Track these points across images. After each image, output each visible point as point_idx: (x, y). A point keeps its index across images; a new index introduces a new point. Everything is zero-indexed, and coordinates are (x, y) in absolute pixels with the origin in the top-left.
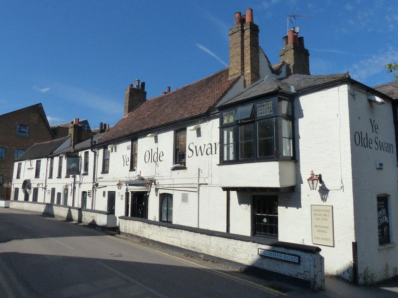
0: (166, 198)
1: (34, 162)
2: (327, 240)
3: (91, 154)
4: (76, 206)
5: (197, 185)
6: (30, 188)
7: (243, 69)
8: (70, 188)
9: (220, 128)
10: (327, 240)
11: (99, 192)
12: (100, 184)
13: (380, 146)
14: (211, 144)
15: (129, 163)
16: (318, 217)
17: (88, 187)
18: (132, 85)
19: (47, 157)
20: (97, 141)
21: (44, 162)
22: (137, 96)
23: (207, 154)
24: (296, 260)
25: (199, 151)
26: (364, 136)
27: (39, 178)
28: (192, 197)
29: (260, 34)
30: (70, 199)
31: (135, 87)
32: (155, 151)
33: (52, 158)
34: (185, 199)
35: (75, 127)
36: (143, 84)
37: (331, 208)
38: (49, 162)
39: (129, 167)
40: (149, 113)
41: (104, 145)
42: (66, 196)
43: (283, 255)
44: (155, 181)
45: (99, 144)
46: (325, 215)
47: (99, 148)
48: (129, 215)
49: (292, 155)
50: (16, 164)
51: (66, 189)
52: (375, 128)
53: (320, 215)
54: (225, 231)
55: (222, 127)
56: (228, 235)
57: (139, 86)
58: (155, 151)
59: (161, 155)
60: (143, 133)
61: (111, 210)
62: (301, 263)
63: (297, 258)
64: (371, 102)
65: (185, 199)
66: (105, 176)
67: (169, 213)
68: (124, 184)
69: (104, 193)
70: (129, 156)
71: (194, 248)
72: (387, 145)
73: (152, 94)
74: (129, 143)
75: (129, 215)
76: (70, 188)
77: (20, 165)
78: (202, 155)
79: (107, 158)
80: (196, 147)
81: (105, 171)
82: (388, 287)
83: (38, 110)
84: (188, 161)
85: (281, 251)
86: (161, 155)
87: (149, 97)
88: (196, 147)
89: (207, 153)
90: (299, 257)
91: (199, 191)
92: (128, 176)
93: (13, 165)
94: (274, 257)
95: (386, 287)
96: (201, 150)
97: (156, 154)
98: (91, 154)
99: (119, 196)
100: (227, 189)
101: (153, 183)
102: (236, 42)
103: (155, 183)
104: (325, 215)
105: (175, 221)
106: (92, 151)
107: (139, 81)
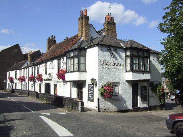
1: (15, 71)
3: (68, 60)
6: (13, 83)
7: (82, 34)
18: (49, 38)
19: (19, 69)
21: (18, 71)
22: (52, 42)
31: (51, 38)
33: (21, 70)
34: (60, 86)
35: (30, 55)
36: (55, 37)
38: (20, 71)
41: (46, 62)
45: (36, 64)
47: (36, 66)
50: (8, 73)
57: (52, 38)
72: (119, 64)
73: (58, 41)
77: (9, 73)
82: (45, 113)
83: (17, 47)
87: (57, 42)
93: (7, 73)
95: (43, 113)
107: (53, 36)
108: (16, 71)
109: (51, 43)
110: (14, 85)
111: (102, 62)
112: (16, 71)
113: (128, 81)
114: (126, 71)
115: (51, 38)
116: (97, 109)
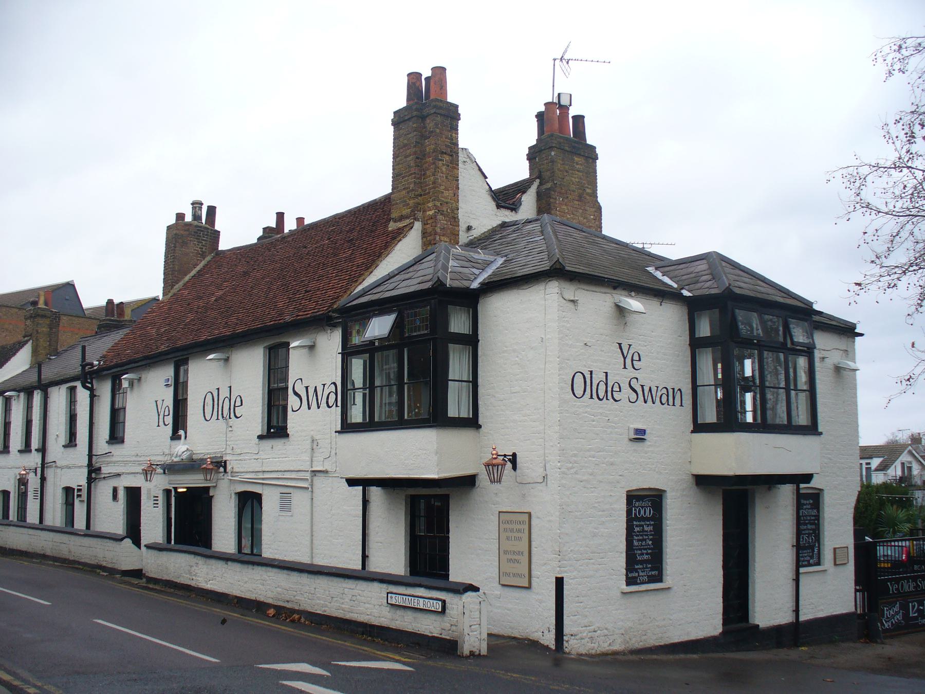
0: (249, 503)
2: (520, 575)
4: (49, 521)
5: (308, 476)
8: (34, 482)
9: (343, 354)
10: (520, 575)
11: (103, 491)
12: (105, 470)
13: (646, 395)
14: (335, 384)
15: (169, 420)
16: (510, 534)
17: (79, 479)
20: (96, 363)
23: (329, 407)
24: (438, 606)
25: (312, 398)
26: (598, 377)
27: (632, 498)
28: (299, 500)
29: (461, 124)
30: (33, 506)
32: (224, 393)
36: (212, 210)
37: (526, 517)
39: (169, 430)
40: (221, 293)
42: (23, 497)
43: (421, 600)
44: (225, 462)
46: (519, 531)
48: (173, 542)
49: (471, 417)
51: (22, 482)
52: (630, 358)
53: (512, 530)
54: (359, 567)
55: (348, 352)
56: (363, 575)
58: (224, 393)
59: (238, 403)
60: (203, 348)
61: (133, 531)
62: (447, 611)
63: (440, 603)
64: (621, 311)
65: (285, 505)
66: (117, 450)
67: (256, 536)
68: (160, 470)
69: (115, 490)
70: (170, 402)
71: (288, 601)
74: (168, 372)
75: (173, 542)
76: (34, 482)
78: (319, 407)
79: (121, 406)
80: (307, 388)
81: (116, 437)
84: (294, 422)
85: (420, 594)
86: (238, 403)
87: (225, 244)
88: (307, 388)
89: (327, 403)
90: (444, 602)
91: (312, 485)
92: (167, 452)
94: (410, 606)
96: (317, 396)
97: (227, 401)
98: (83, 395)
99: (149, 498)
100: (365, 483)
101: (222, 469)
102: (406, 142)
103: (225, 467)
104: (519, 531)
105: (268, 551)
106: (85, 387)
109: (193, 247)
115: (188, 218)
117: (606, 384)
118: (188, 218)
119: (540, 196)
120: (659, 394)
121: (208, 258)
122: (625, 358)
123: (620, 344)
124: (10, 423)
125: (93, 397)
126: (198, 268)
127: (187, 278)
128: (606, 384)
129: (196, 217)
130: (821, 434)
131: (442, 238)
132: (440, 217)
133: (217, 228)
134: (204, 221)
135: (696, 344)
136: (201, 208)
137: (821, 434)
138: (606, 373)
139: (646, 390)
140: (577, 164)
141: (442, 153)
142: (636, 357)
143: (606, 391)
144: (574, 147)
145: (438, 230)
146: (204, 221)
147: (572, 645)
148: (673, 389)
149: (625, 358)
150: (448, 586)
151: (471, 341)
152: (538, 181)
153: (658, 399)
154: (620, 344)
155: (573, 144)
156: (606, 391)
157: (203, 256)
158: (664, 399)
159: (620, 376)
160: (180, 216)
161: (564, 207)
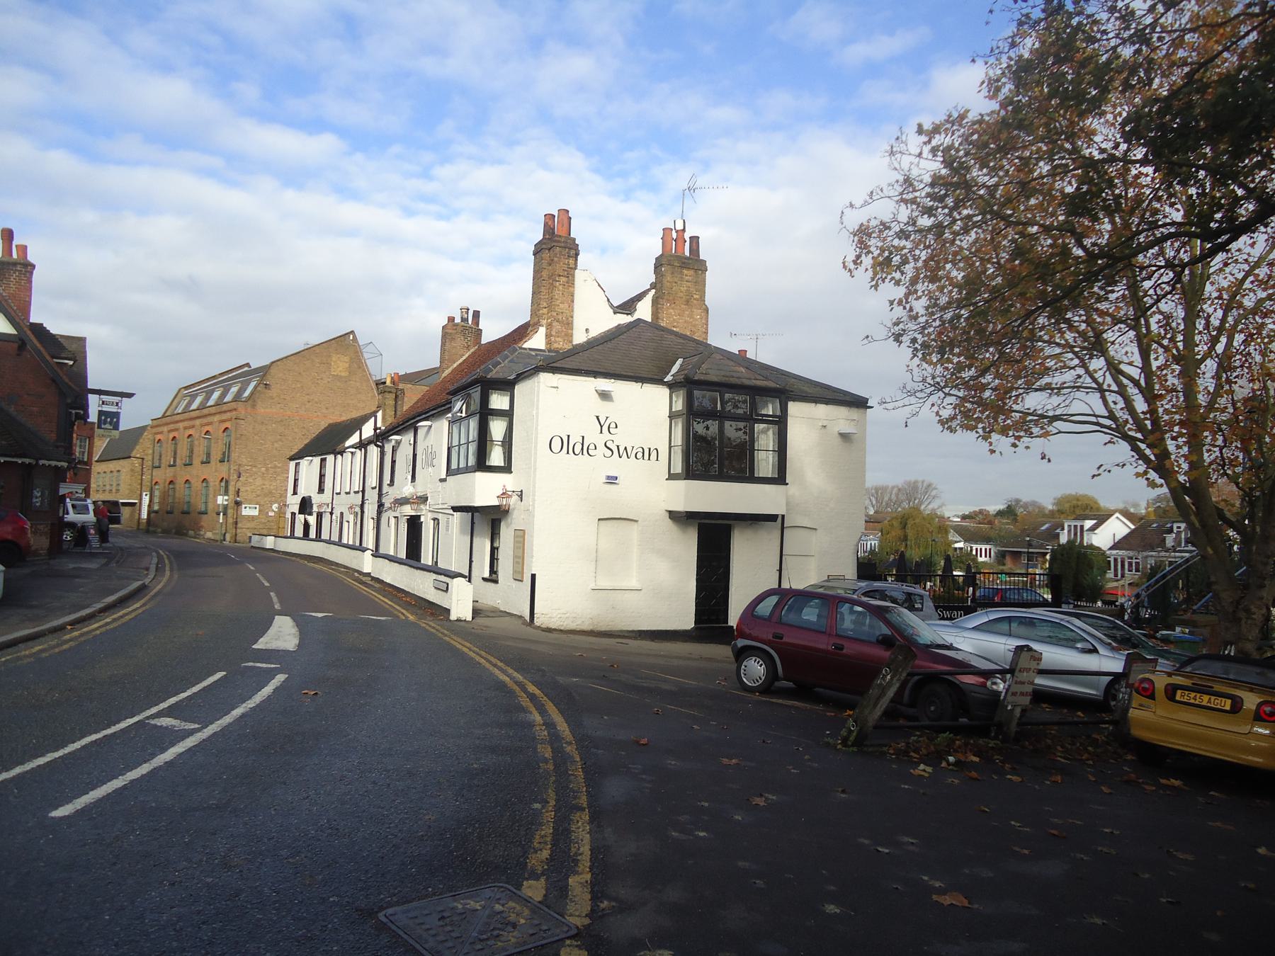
36: (477, 314)
90: (448, 584)
108: (323, 461)
109: (460, 341)
110: (312, 520)
111: (556, 444)
112: (323, 461)
113: (681, 518)
114: (672, 477)
115: (458, 320)
116: (528, 618)
117: (583, 444)
118: (458, 320)
119: (655, 302)
120: (634, 452)
121: (472, 350)
122: (601, 427)
123: (597, 417)
124: (324, 475)
125: (382, 454)
126: (464, 358)
127: (455, 365)
128: (583, 444)
129: (464, 320)
130: (787, 484)
131: (557, 339)
132: (555, 324)
133: (480, 327)
134: (470, 322)
135: (672, 416)
136: (467, 313)
137: (787, 484)
138: (583, 437)
139: (622, 449)
140: (686, 275)
141: (560, 276)
142: (613, 425)
143: (582, 449)
144: (684, 263)
145: (553, 333)
146: (470, 322)
147: (537, 622)
148: (650, 449)
149: (601, 427)
150: (419, 566)
151: (508, 414)
152: (653, 291)
153: (633, 455)
154: (597, 417)
155: (684, 260)
156: (582, 449)
157: (468, 348)
158: (640, 455)
159: (593, 436)
160: (451, 319)
161: (672, 311)
